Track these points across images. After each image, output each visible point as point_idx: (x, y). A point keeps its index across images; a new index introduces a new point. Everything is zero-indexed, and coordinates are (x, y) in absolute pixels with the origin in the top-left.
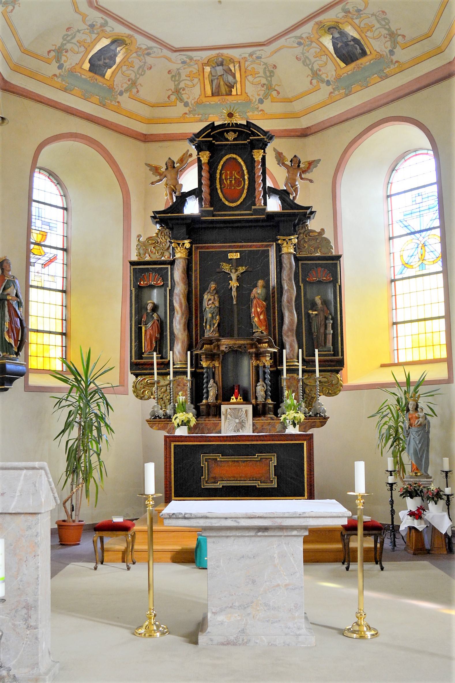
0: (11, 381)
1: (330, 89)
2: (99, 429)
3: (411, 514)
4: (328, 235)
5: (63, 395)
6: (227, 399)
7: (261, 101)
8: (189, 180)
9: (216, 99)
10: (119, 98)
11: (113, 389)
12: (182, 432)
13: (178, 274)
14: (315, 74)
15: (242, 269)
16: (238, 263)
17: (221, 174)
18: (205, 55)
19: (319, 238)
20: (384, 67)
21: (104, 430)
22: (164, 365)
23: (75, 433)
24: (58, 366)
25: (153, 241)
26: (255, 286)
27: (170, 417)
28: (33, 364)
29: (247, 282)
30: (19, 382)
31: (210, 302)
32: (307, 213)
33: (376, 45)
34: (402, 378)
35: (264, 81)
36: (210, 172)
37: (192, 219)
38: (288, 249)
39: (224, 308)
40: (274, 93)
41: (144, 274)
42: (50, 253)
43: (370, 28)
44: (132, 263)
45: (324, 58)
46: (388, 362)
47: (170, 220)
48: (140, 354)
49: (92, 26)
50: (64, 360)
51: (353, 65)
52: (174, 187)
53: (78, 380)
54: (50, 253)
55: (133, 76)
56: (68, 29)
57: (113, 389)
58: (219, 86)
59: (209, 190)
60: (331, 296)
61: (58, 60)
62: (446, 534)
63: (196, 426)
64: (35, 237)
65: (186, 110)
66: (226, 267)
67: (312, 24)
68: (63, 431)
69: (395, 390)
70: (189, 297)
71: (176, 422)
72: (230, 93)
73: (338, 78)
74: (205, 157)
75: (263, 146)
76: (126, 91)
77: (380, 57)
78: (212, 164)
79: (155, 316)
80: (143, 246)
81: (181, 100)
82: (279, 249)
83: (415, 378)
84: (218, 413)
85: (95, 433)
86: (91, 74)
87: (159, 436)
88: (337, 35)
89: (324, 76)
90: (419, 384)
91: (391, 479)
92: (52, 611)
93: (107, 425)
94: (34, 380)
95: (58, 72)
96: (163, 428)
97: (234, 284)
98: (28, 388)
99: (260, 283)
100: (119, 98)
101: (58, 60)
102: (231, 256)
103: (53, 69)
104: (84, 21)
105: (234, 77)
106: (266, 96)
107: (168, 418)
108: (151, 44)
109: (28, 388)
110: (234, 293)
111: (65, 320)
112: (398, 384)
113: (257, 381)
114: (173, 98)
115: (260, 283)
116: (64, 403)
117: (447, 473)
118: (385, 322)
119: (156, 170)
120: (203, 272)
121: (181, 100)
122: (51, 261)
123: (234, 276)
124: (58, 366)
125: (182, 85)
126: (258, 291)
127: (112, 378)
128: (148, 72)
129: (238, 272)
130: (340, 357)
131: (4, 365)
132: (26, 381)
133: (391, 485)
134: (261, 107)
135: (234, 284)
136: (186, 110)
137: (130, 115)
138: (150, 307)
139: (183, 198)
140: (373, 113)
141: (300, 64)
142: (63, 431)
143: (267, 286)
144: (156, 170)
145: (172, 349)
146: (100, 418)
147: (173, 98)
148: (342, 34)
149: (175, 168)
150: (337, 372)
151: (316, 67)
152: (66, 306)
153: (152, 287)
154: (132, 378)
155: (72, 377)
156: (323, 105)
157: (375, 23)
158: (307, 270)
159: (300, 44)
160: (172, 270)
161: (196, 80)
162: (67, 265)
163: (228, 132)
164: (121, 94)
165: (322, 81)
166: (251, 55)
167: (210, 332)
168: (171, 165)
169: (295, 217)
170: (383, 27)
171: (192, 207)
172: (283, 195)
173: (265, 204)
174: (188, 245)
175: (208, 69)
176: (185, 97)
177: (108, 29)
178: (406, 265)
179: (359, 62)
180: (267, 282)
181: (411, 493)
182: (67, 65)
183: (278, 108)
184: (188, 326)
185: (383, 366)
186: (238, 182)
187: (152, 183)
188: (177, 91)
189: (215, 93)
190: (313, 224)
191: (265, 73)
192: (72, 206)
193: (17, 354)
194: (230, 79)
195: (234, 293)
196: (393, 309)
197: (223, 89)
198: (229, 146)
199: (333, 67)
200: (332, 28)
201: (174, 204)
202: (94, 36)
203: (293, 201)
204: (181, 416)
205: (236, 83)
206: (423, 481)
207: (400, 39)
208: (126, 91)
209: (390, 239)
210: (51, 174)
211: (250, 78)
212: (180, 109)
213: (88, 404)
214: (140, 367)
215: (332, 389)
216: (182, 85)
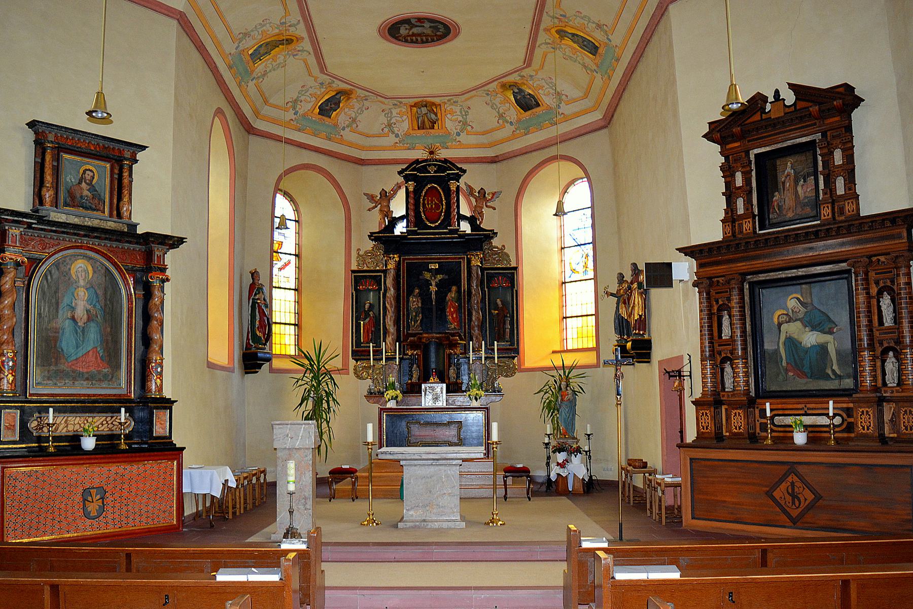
0: (260, 366)
1: (513, 128)
2: (328, 402)
3: (558, 464)
4: (510, 251)
5: (300, 376)
6: (426, 380)
7: (458, 134)
8: (399, 207)
9: (422, 131)
10: (342, 132)
11: (338, 371)
12: (391, 404)
13: (390, 282)
14: (501, 116)
15: (439, 277)
16: (437, 272)
17: (424, 200)
18: (412, 101)
19: (502, 254)
20: (554, 117)
21: (331, 403)
22: (378, 352)
23: (310, 405)
24: (291, 351)
25: (371, 254)
26: (450, 291)
27: (383, 393)
28: (276, 350)
29: (444, 288)
30: (266, 366)
31: (415, 303)
32: (490, 235)
33: (547, 100)
34: (558, 363)
35: (460, 118)
36: (413, 200)
37: (402, 237)
38: (476, 262)
39: (426, 309)
40: (469, 128)
41: (362, 281)
42: (285, 258)
43: (542, 87)
44: (353, 272)
45: (507, 105)
46: (558, 349)
47: (385, 239)
48: (358, 343)
49: (322, 84)
50: (298, 344)
51: (529, 112)
52: (387, 213)
53: (314, 368)
54: (285, 258)
55: (353, 115)
56: (303, 86)
57: (338, 371)
58: (423, 122)
59: (414, 215)
60: (509, 298)
61: (294, 108)
62: (583, 479)
63: (402, 401)
64: (276, 247)
65: (397, 140)
66: (427, 275)
67: (496, 83)
68: (301, 404)
69: (554, 373)
70: (397, 298)
71: (387, 397)
72: (433, 128)
73: (519, 121)
74: (411, 185)
75: (457, 178)
76: (348, 126)
77: (549, 108)
78: (417, 191)
79: (371, 313)
80: (362, 258)
81: (393, 132)
82: (469, 261)
83: (568, 363)
84: (419, 391)
85: (325, 405)
86: (320, 116)
87: (375, 408)
88: (516, 91)
89: (508, 118)
90: (572, 368)
91: (546, 440)
92: (318, 495)
93: (334, 399)
94: (276, 363)
95: (293, 117)
96: (377, 402)
97: (433, 288)
98: (272, 370)
99: (454, 288)
100: (342, 132)
101: (294, 108)
102: (432, 266)
103: (290, 115)
104: (315, 81)
105: (436, 115)
106: (462, 131)
107: (382, 394)
108: (367, 94)
109: (272, 370)
110: (433, 296)
111: (298, 314)
112: (555, 368)
113: (450, 366)
114: (386, 130)
115: (454, 288)
116: (300, 382)
117: (589, 435)
118: (556, 316)
119: (371, 198)
120: (412, 278)
121: (393, 132)
122: (286, 265)
123: (434, 283)
124: (291, 351)
125: (393, 121)
126: (452, 295)
127: (338, 363)
128: (365, 112)
129: (437, 280)
130: (516, 346)
131: (256, 354)
132: (271, 366)
133: (547, 444)
134: (458, 138)
135: (433, 288)
136: (397, 140)
137: (350, 145)
138: (367, 306)
139: (394, 222)
140: (546, 150)
141: (489, 108)
142: (301, 404)
143: (459, 291)
144: (371, 198)
145: (385, 341)
146: (328, 394)
147: (386, 130)
148: (521, 91)
149: (386, 197)
150: (513, 358)
151: (501, 111)
152: (298, 302)
153: (371, 290)
154: (352, 363)
155: (307, 362)
156: (508, 139)
157: (544, 84)
158: (490, 278)
159: (488, 94)
160: (385, 277)
161: (405, 117)
162: (299, 268)
163: (429, 165)
164: (344, 129)
165: (507, 122)
166: (449, 100)
167: (415, 327)
168: (384, 194)
169: (481, 239)
170: (551, 88)
171: (400, 229)
172: (472, 220)
173: (459, 225)
174: (397, 259)
175: (415, 109)
176: (396, 130)
177: (334, 85)
178: (573, 271)
179: (534, 110)
180: (459, 288)
181: (560, 450)
182: (301, 112)
183: (472, 139)
184: (397, 322)
185: (554, 352)
186: (437, 207)
187: (369, 210)
188: (389, 125)
189: (422, 127)
190: (495, 242)
191: (461, 112)
192: (304, 219)
193: (265, 344)
194: (433, 116)
195: (433, 296)
196: (563, 306)
197: (427, 124)
198: (432, 181)
199: (513, 112)
200: (512, 86)
201: (386, 227)
202: (323, 90)
203: (479, 226)
204: (391, 393)
205: (437, 120)
206: (570, 441)
207: (564, 97)
208: (348, 126)
209: (562, 248)
210: (286, 194)
211: (449, 116)
212: (392, 139)
213: (319, 383)
214: (359, 354)
215: (510, 372)
216: (393, 121)
